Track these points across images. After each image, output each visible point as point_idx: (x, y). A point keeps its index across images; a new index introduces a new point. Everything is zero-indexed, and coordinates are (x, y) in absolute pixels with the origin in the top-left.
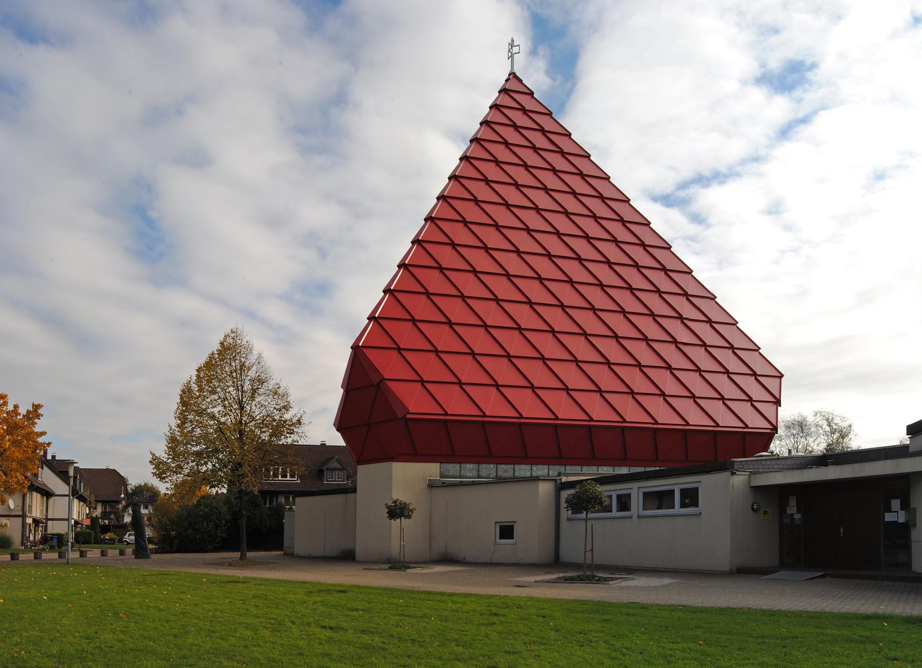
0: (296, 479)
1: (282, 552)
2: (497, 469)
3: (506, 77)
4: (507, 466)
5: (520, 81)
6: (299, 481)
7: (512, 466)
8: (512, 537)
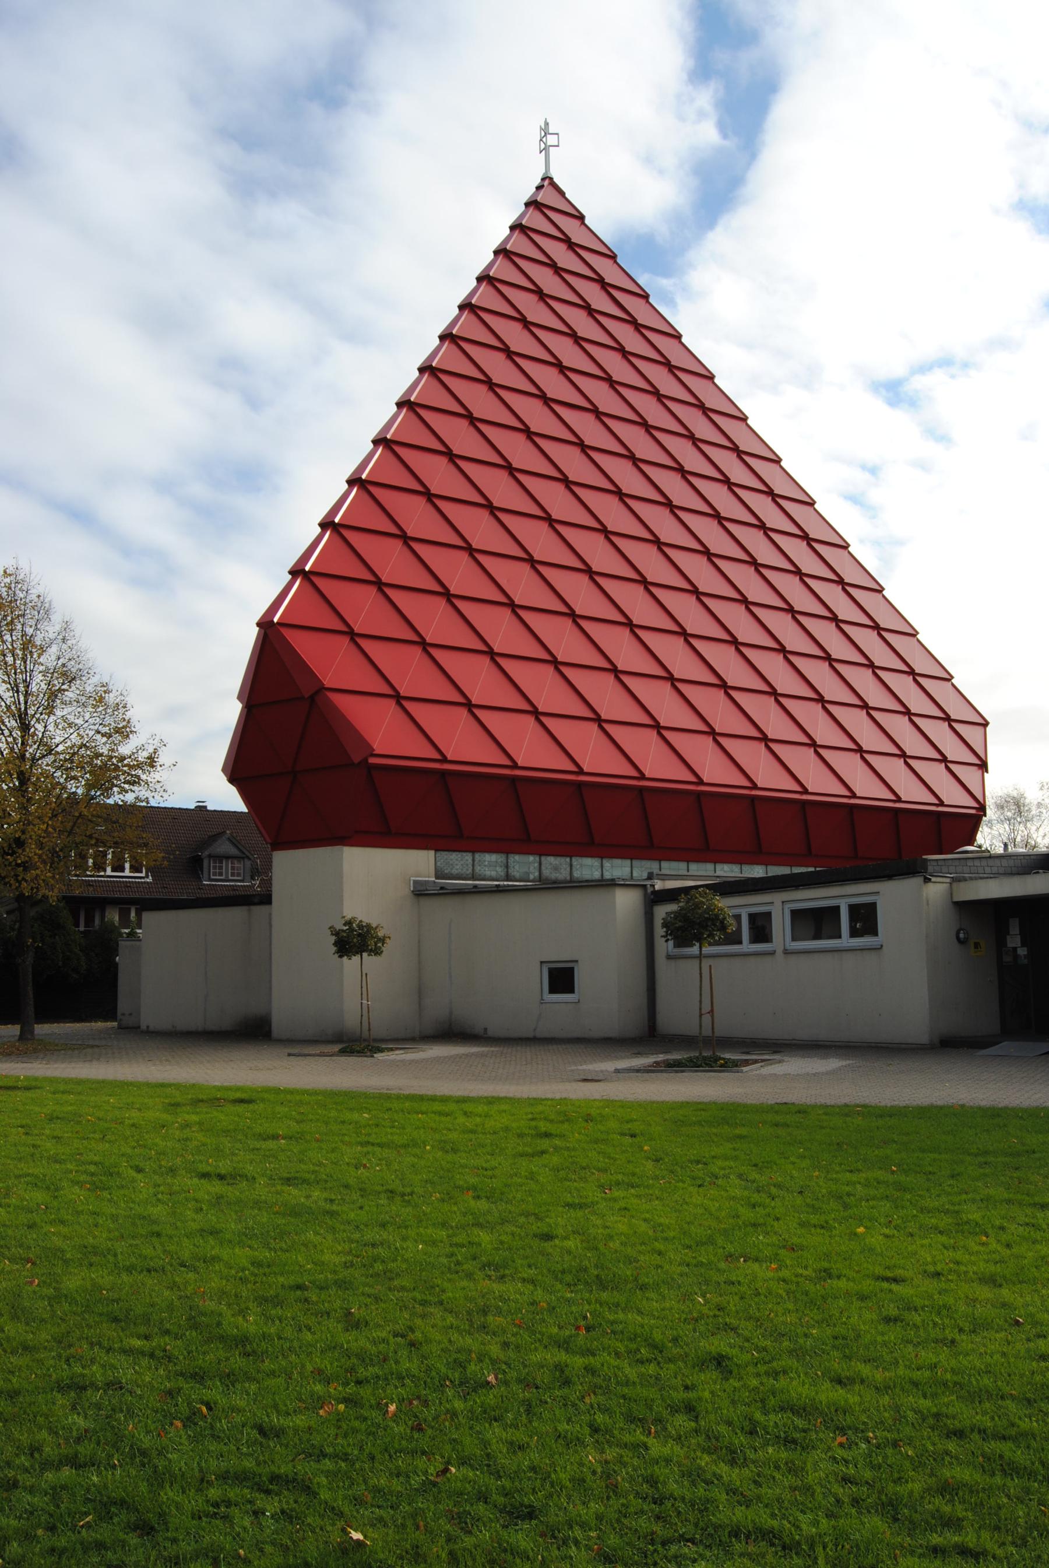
0: (143, 875)
1: (115, 1024)
2: (540, 864)
3: (537, 181)
4: (559, 859)
5: (562, 193)
6: (150, 879)
7: (568, 859)
8: (571, 990)
